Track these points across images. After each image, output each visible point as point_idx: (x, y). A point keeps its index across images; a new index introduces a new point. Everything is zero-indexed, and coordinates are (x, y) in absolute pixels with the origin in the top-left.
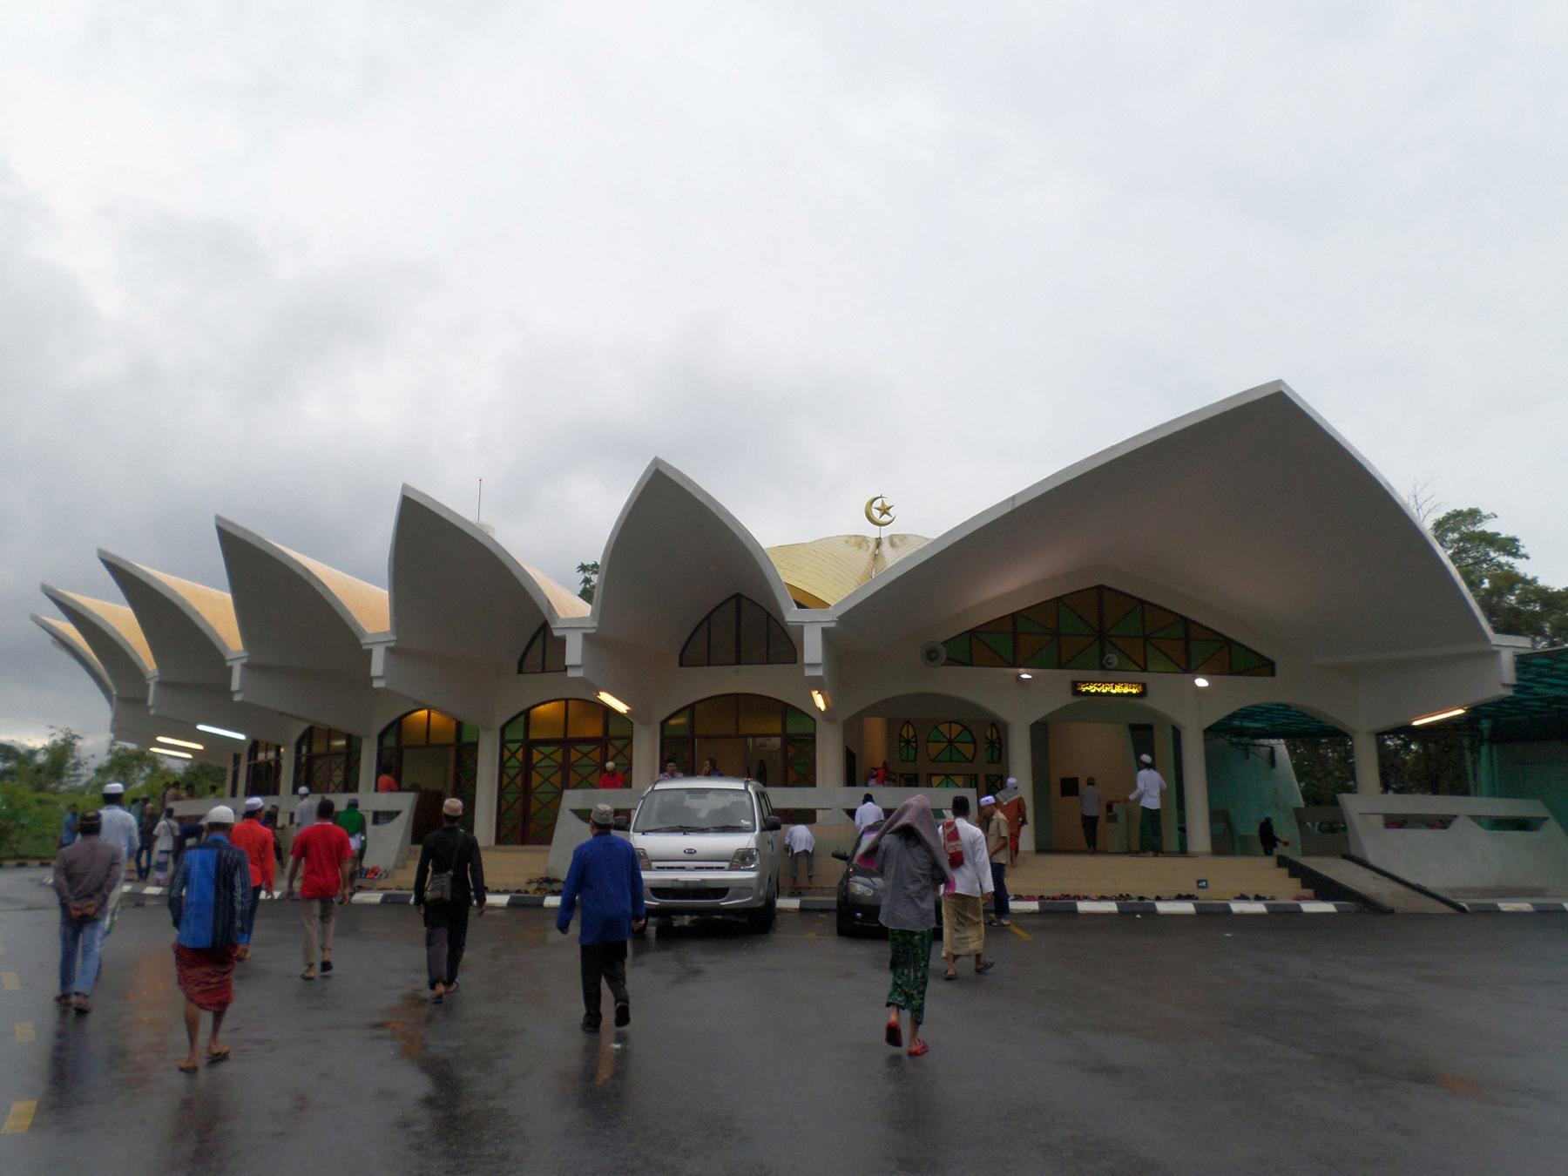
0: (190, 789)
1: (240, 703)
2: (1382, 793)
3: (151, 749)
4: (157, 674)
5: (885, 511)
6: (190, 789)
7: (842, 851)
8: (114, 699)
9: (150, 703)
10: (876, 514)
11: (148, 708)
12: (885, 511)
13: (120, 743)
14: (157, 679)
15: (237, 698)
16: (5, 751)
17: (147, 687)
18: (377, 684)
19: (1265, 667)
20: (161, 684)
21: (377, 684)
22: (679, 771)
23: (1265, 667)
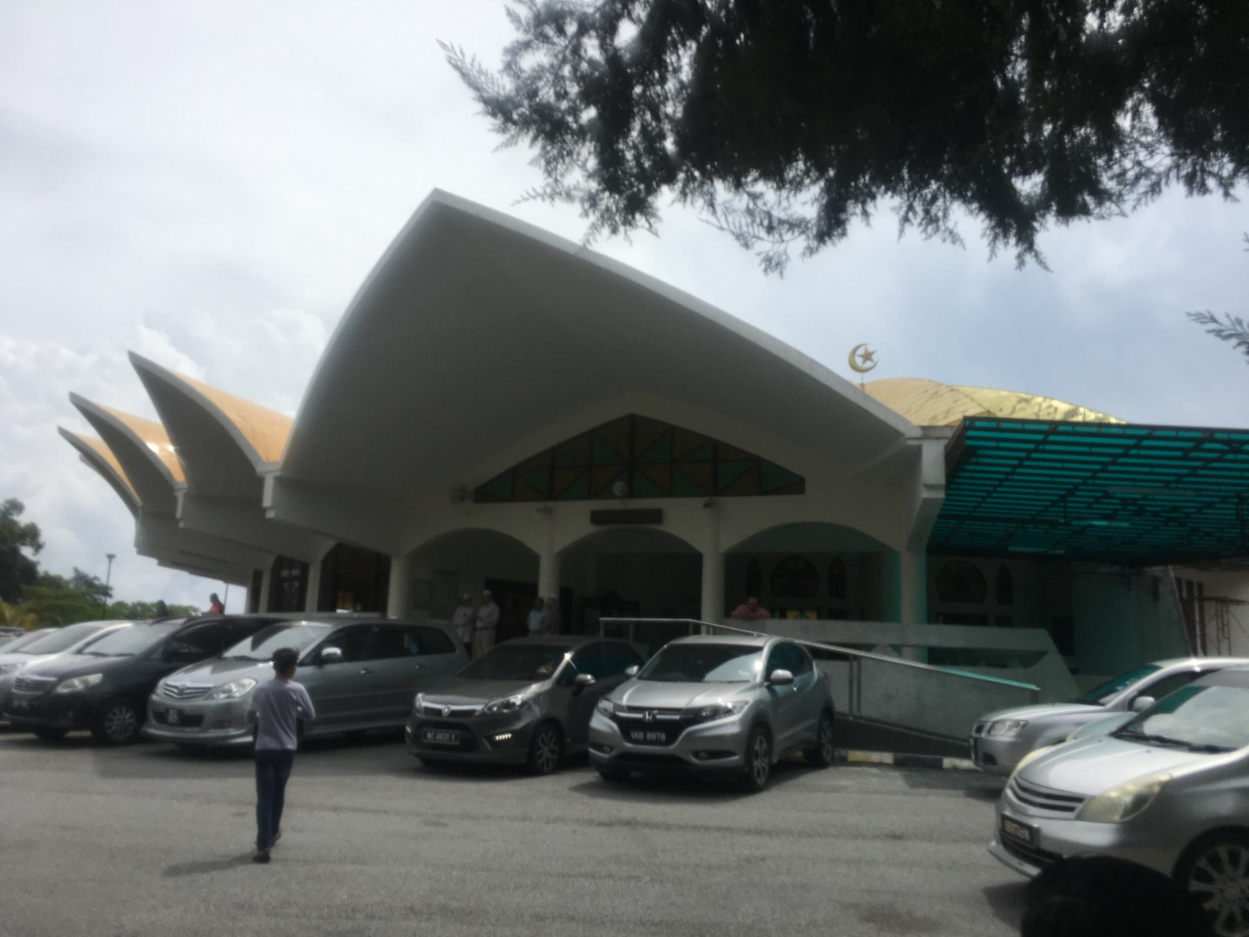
0: (740, 237)
1: (271, 521)
2: (1187, 196)
3: (510, 735)
4: (185, 486)
5: (867, 356)
6: (740, 237)
7: (779, 275)
8: (140, 511)
9: (179, 514)
10: (859, 361)
11: (177, 521)
12: (867, 356)
13: (406, 645)
14: (185, 491)
15: (181, 525)
16: (2, 725)
17: (175, 500)
18: (270, 515)
19: (792, 485)
20: (188, 496)
21: (270, 515)
22: (1206, 157)
23: (792, 485)
